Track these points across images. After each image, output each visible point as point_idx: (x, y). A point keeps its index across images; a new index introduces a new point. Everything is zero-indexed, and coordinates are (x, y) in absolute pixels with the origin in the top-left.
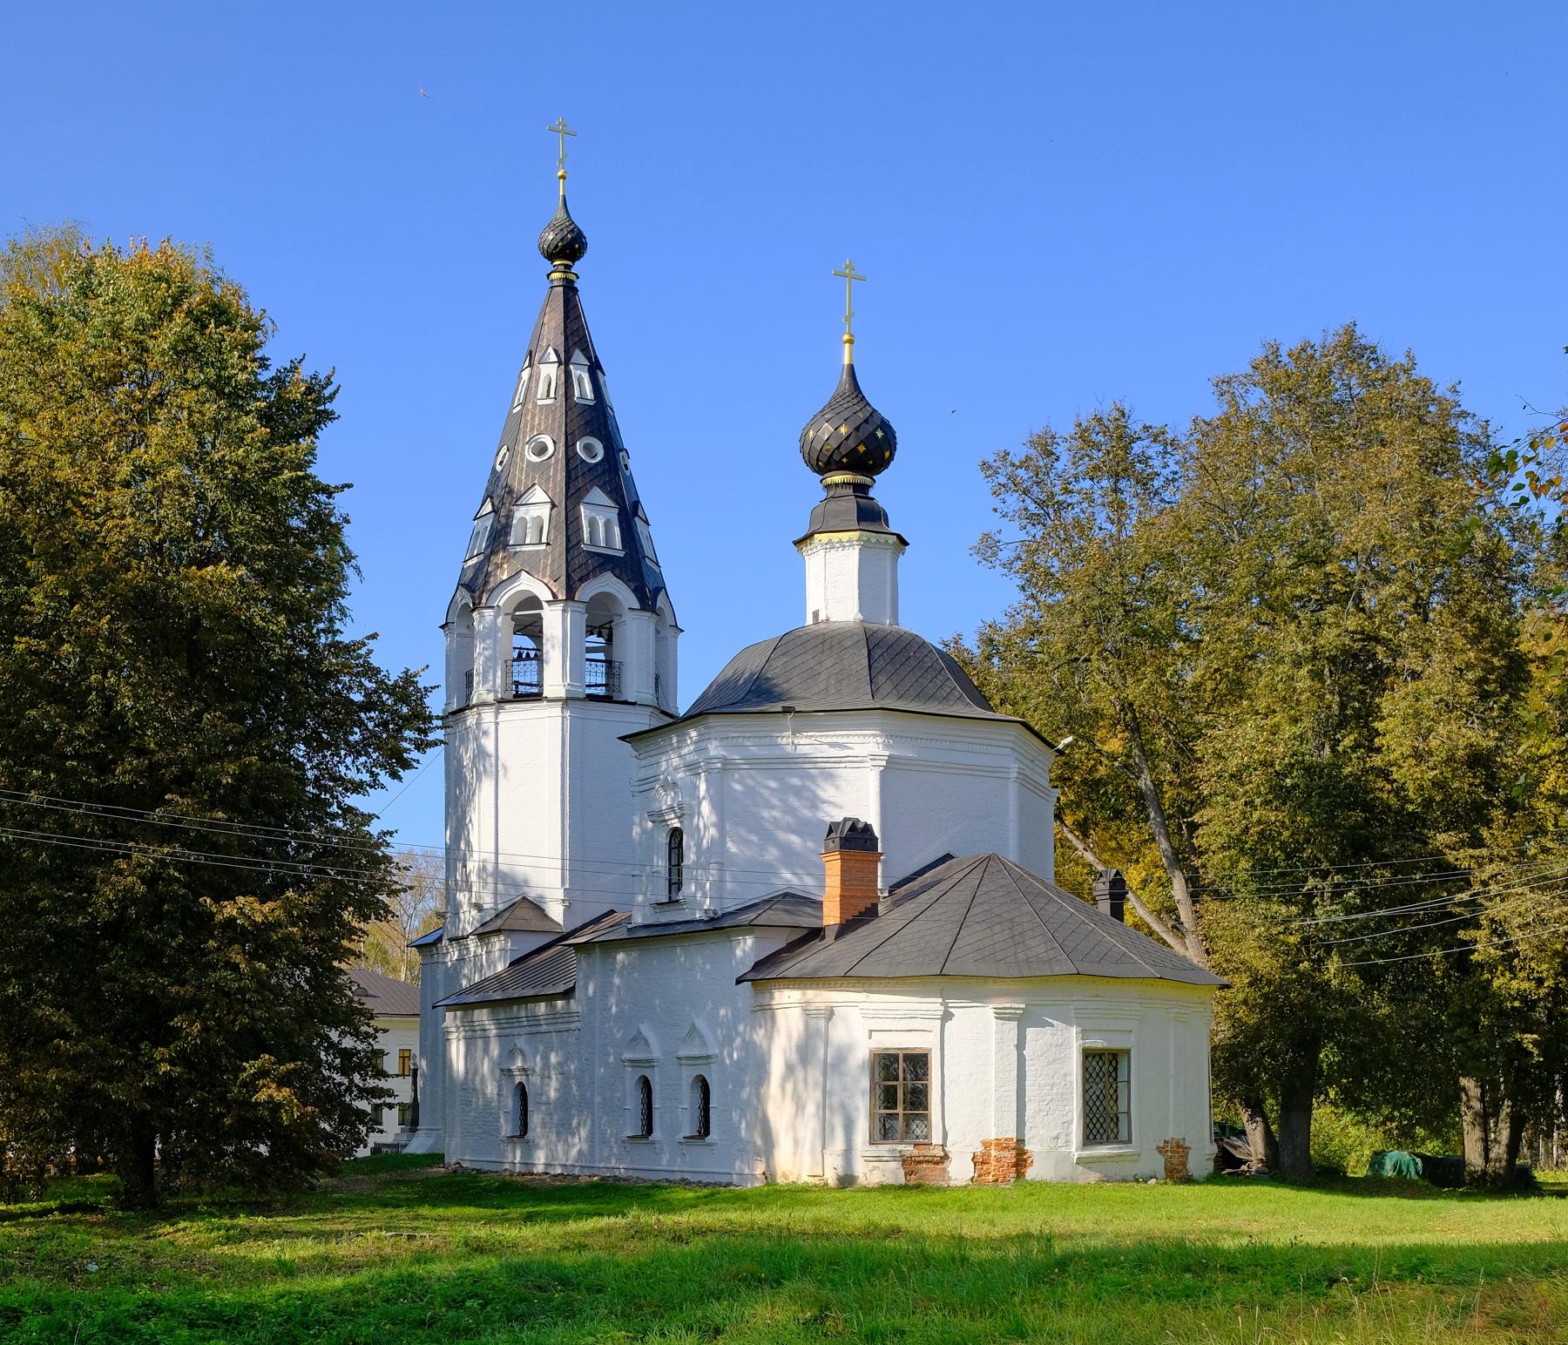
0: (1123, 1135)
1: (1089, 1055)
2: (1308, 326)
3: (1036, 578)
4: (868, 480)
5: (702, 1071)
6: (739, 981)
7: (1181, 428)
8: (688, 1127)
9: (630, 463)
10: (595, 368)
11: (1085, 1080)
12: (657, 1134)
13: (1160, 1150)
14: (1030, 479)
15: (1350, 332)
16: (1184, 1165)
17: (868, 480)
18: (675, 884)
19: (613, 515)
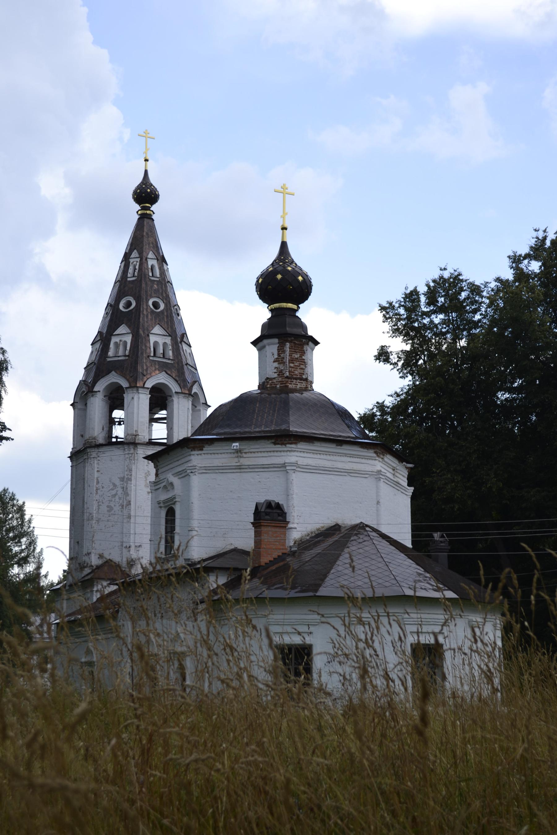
4: (295, 307)
10: (162, 260)
14: (406, 315)
17: (295, 307)
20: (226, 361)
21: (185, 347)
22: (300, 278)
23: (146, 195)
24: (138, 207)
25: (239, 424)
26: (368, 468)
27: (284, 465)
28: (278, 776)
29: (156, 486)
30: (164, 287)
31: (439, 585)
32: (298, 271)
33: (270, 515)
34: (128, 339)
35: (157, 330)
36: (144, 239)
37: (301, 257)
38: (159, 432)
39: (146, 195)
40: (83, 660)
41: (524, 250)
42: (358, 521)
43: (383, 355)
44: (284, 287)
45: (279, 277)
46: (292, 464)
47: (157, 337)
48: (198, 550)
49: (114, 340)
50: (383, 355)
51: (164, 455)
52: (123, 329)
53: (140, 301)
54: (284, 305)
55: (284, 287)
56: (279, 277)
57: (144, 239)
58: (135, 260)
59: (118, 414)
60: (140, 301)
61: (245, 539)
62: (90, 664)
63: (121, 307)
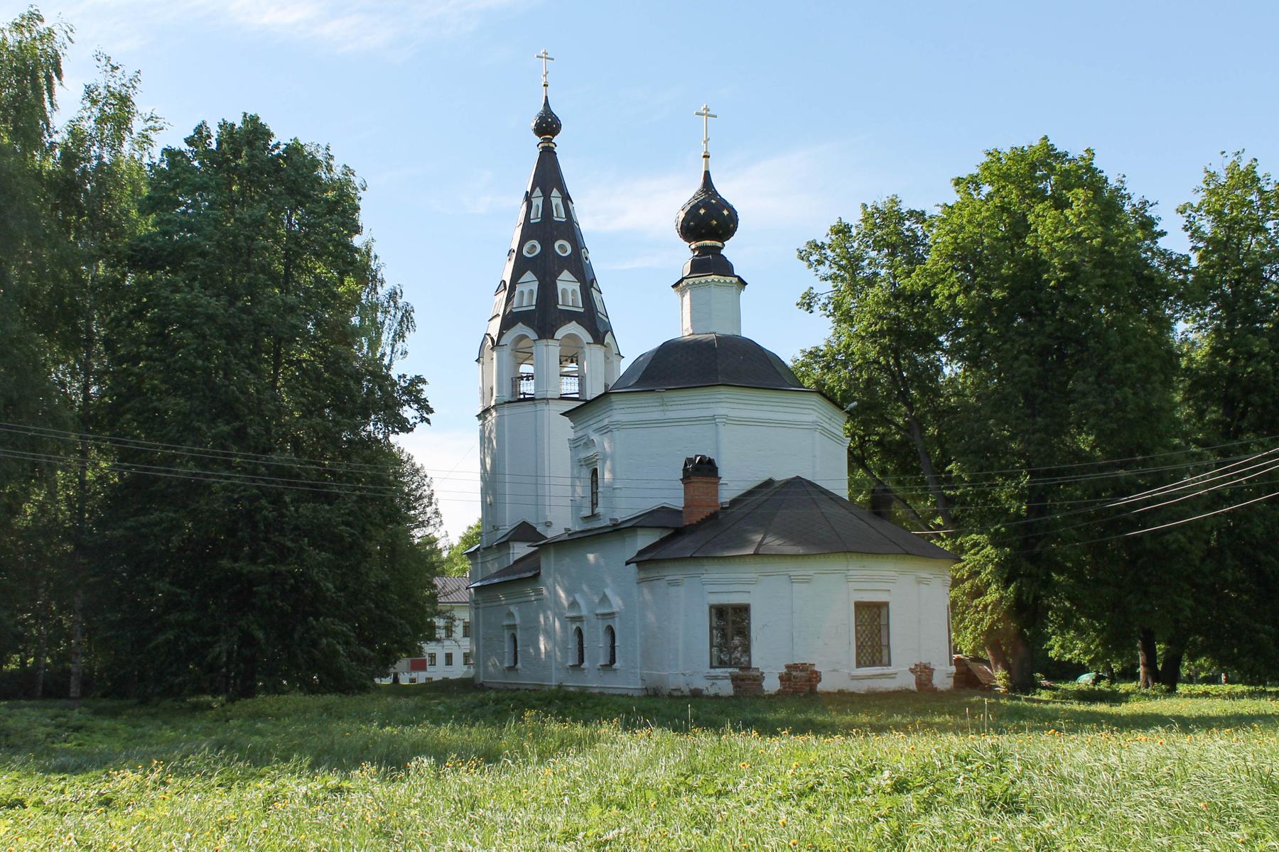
0: (885, 659)
1: (860, 607)
2: (1020, 136)
3: (845, 317)
4: (719, 244)
5: (610, 622)
6: (627, 563)
7: (933, 210)
8: (603, 660)
9: (589, 256)
10: (566, 198)
11: (856, 626)
12: (586, 664)
13: (912, 670)
14: (842, 254)
15: (1046, 138)
16: (930, 680)
17: (719, 244)
18: (594, 504)
19: (577, 286)
20: (646, 307)
21: (595, 293)
22: (726, 212)
23: (547, 126)
24: (539, 140)
25: (677, 368)
26: (805, 418)
27: (713, 418)
28: (265, 513)
29: (575, 444)
30: (570, 230)
31: (129, 524)
32: (724, 204)
33: (701, 470)
34: (535, 286)
35: (566, 275)
36: (548, 175)
37: (725, 189)
38: (570, 386)
39: (547, 126)
40: (505, 623)
41: (806, 264)
42: (766, 478)
43: (807, 302)
44: (709, 223)
45: (702, 211)
46: (721, 416)
47: (567, 285)
48: (624, 508)
49: (519, 288)
50: (807, 302)
51: (582, 409)
52: (529, 276)
53: (552, 240)
54: (708, 242)
55: (709, 223)
56: (702, 211)
57: (548, 175)
58: (538, 202)
59: (526, 369)
60: (552, 240)
61: (676, 499)
62: (513, 627)
63: (525, 253)
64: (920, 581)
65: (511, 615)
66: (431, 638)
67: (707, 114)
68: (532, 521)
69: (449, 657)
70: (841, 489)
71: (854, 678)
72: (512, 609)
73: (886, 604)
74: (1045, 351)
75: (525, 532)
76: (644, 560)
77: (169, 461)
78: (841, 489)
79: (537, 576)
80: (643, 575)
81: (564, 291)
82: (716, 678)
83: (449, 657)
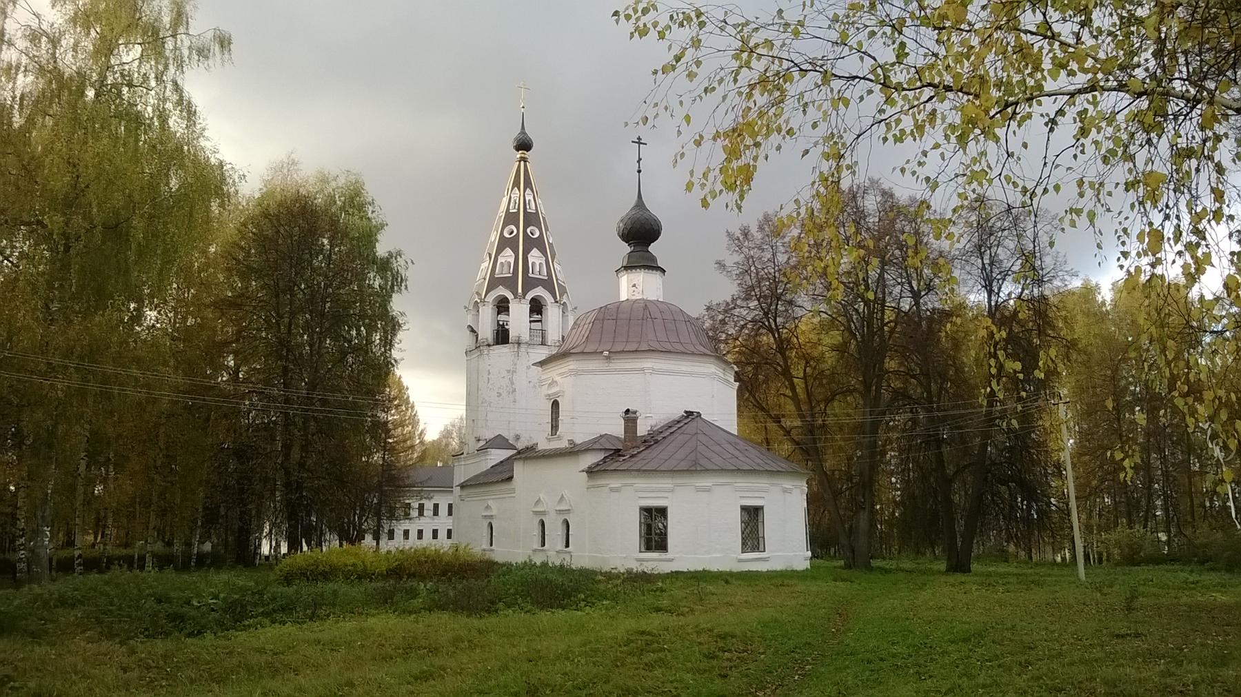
46: (649, 368)
64: (785, 491)
65: (488, 507)
66: (407, 516)
67: (639, 142)
68: (505, 434)
69: (420, 532)
70: (734, 430)
71: (740, 561)
72: (490, 503)
73: (761, 508)
74: (776, 621)
75: (499, 442)
76: (591, 472)
77: (103, 315)
78: (734, 430)
79: (510, 478)
80: (591, 483)
81: (533, 264)
82: (643, 560)
83: (420, 532)
